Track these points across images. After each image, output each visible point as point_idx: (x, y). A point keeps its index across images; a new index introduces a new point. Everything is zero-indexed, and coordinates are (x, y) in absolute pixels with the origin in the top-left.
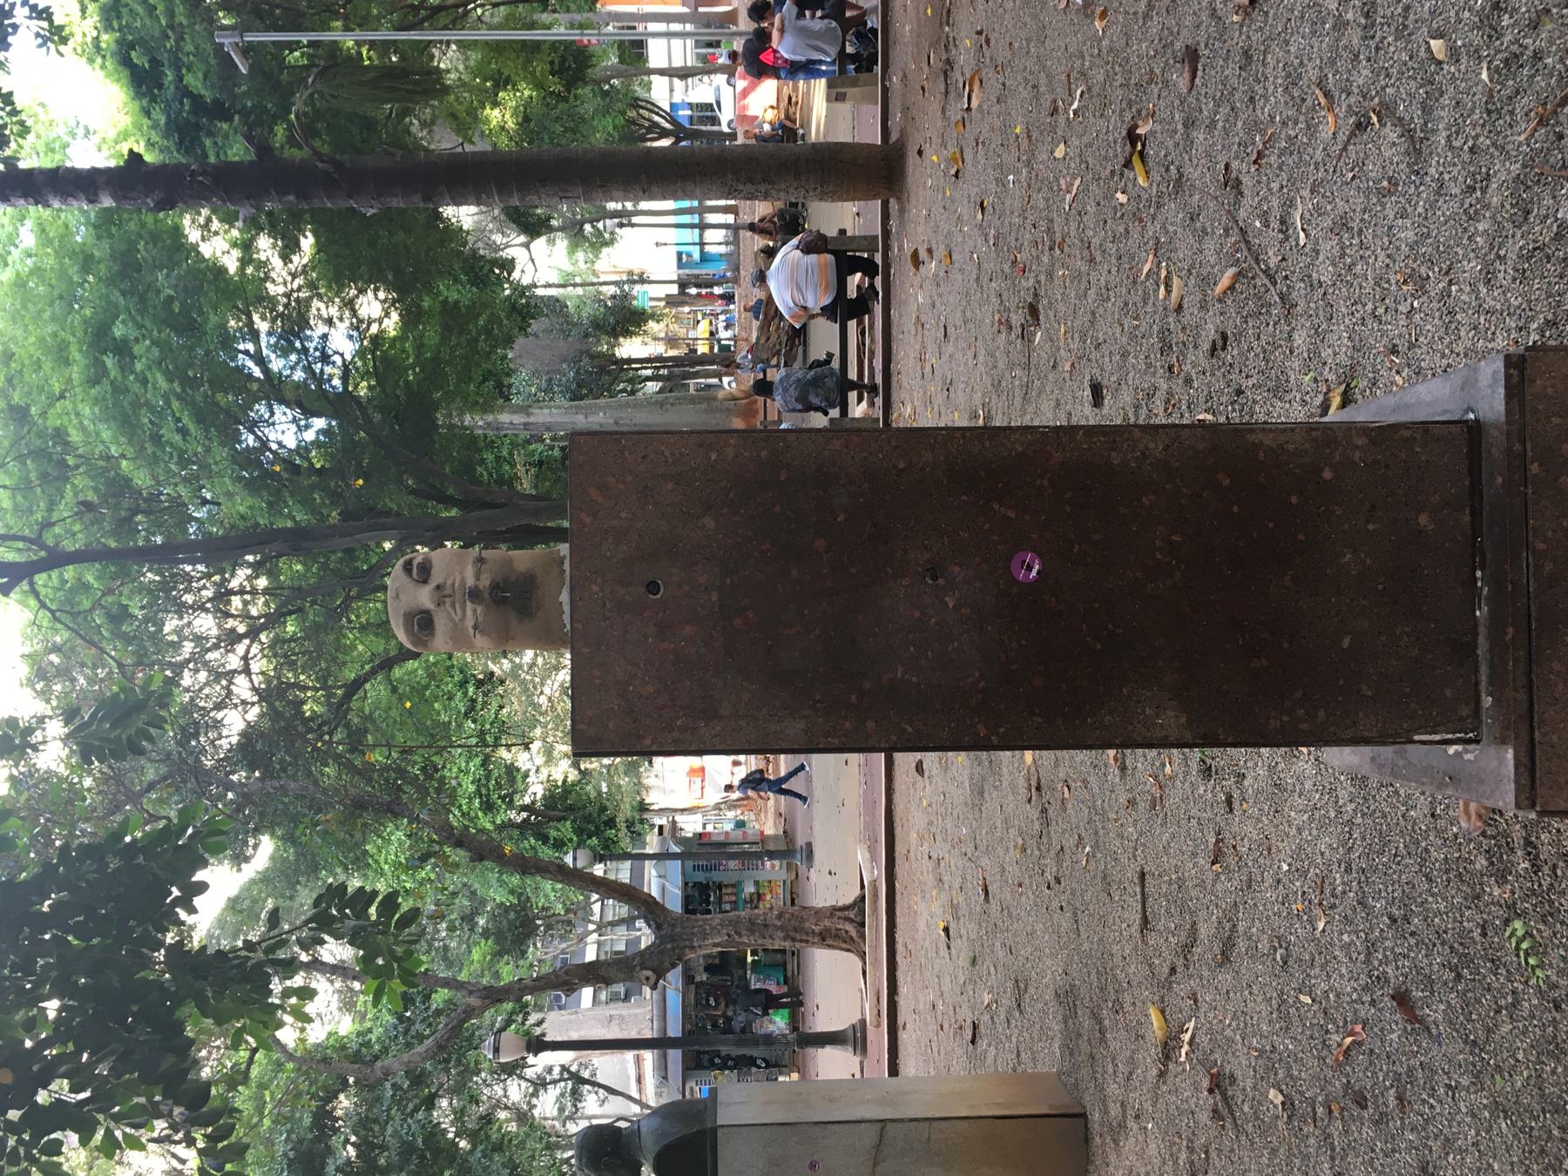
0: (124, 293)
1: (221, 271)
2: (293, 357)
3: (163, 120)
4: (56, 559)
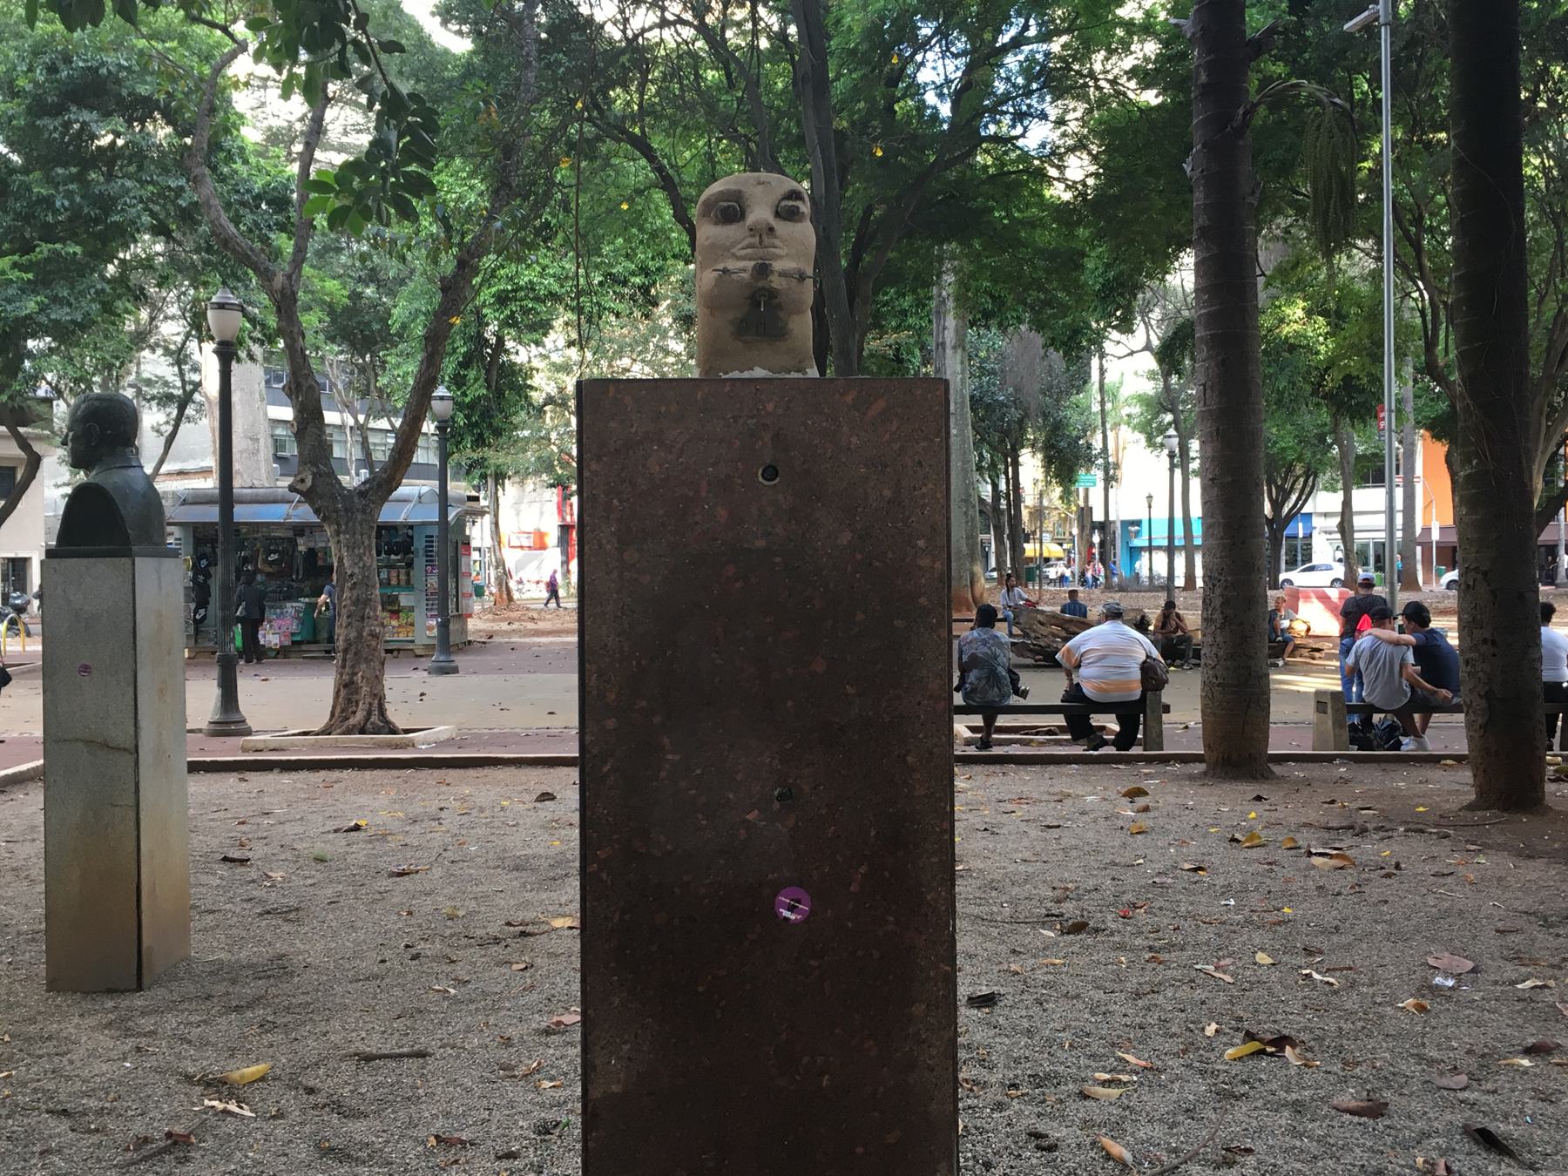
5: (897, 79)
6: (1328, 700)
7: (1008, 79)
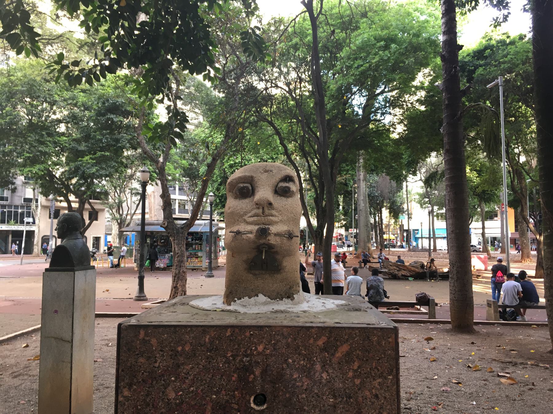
0: (406, 47)
1: (413, 79)
2: (383, 103)
3: (466, 60)
4: (315, 27)
5: (346, 103)
6: (492, 303)
7: (379, 103)
